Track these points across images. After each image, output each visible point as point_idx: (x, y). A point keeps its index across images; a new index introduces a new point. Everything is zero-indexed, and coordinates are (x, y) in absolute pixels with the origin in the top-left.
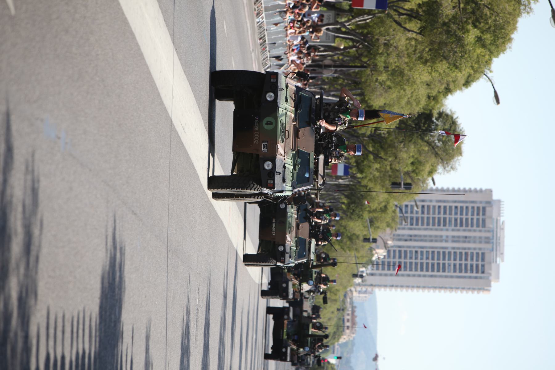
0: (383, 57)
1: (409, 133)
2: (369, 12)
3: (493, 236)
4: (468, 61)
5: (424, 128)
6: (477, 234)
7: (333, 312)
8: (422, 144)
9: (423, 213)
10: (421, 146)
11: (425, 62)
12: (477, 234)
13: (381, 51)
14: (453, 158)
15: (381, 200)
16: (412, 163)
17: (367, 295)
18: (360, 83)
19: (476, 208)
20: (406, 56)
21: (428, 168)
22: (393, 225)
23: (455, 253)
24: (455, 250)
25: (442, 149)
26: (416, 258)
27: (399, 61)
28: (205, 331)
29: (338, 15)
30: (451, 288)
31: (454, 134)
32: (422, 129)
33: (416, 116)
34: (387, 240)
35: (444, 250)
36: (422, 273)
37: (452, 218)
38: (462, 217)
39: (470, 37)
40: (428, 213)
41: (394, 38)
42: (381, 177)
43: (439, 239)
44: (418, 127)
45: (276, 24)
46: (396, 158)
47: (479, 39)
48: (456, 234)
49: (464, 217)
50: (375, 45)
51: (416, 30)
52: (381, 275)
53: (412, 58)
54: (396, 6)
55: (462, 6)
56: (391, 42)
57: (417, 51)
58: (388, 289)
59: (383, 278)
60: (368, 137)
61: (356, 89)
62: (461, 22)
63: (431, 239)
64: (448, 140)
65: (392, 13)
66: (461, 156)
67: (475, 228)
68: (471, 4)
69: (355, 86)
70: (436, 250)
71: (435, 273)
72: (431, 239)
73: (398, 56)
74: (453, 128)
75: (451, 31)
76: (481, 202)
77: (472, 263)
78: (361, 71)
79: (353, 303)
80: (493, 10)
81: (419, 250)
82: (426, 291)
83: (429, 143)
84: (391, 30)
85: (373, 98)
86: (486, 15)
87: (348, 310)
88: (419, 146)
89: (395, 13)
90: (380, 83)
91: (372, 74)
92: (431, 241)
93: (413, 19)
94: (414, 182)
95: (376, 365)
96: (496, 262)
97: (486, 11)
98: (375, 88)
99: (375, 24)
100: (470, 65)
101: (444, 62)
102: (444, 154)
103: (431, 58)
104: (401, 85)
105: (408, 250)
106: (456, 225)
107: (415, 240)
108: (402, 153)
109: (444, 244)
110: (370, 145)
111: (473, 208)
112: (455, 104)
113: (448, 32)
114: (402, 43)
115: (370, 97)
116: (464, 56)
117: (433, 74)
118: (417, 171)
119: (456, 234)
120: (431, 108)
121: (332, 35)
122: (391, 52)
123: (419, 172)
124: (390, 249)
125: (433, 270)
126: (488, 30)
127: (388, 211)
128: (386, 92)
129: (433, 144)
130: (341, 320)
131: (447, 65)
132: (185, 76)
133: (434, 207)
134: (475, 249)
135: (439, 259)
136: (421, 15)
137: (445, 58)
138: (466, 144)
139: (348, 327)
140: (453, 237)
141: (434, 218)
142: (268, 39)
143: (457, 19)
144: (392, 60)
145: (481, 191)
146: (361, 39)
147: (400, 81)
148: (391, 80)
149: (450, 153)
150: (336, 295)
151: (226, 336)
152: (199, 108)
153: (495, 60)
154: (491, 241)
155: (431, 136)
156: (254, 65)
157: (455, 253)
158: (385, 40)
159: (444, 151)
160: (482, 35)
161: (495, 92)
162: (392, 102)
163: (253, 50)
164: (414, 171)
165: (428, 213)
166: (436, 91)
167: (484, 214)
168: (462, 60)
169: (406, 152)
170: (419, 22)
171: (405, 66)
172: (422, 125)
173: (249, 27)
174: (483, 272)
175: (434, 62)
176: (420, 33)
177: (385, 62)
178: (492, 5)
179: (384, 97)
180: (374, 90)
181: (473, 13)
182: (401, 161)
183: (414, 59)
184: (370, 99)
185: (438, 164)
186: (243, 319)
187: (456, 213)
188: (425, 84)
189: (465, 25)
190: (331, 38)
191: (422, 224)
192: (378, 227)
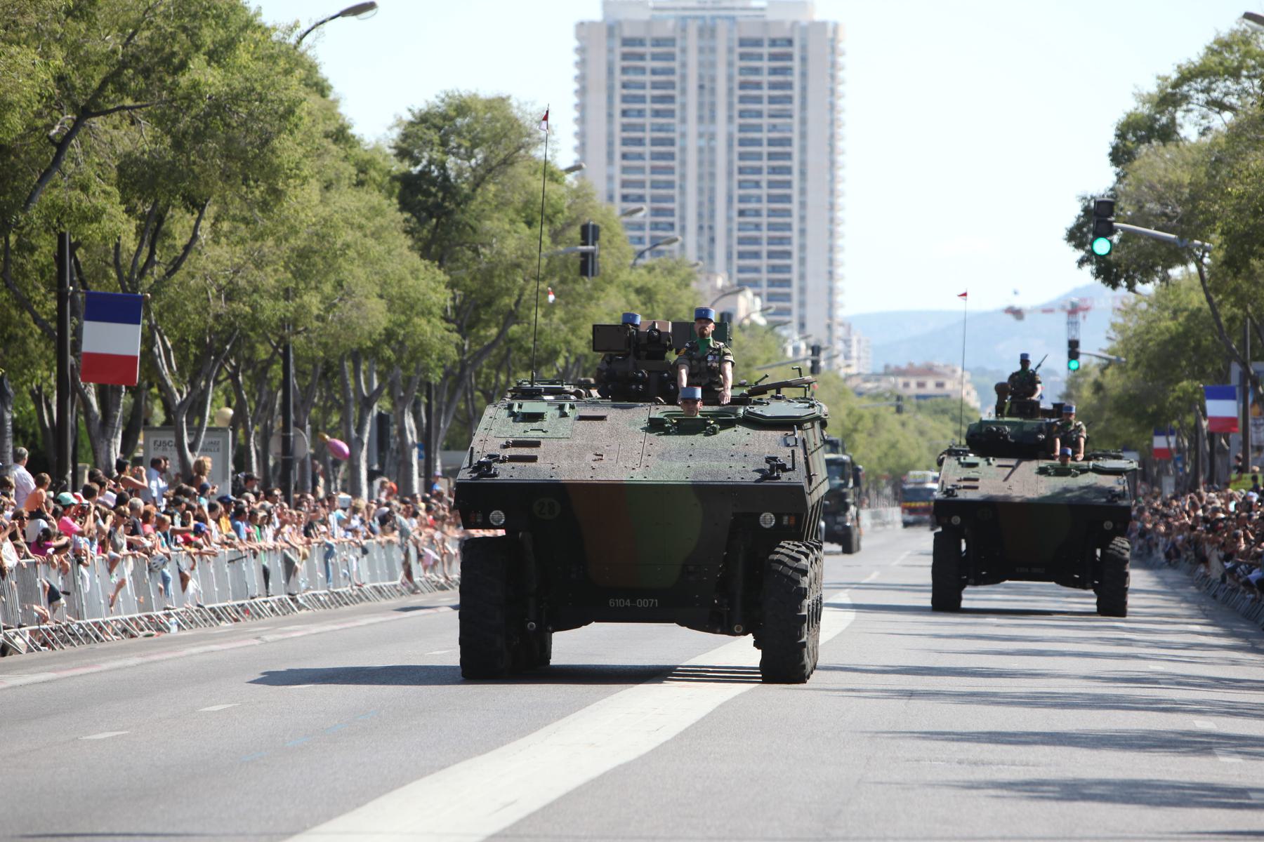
2: (148, 341)
3: (696, 18)
5: (440, 195)
6: (693, 58)
7: (903, 424)
8: (479, 199)
9: (641, 198)
10: (486, 202)
11: (277, 194)
12: (693, 58)
13: (247, 309)
15: (623, 301)
16: (529, 224)
17: (854, 339)
18: (327, 362)
19: (626, 63)
20: (259, 244)
21: (536, 184)
22: (683, 272)
23: (742, 114)
24: (736, 114)
26: (757, 213)
27: (274, 262)
28: (1011, 743)
29: (146, 422)
30: (832, 123)
31: (436, 127)
32: (444, 199)
33: (407, 215)
34: (714, 287)
35: (736, 142)
37: (652, 124)
39: (211, 80)
41: (213, 276)
42: (567, 303)
44: (437, 210)
45: (184, 580)
46: (518, 266)
47: (214, 57)
48: (692, 113)
49: (649, 92)
50: (232, 324)
51: (190, 220)
52: (802, 304)
54: (132, 272)
55: (129, 102)
56: (223, 282)
57: (248, 214)
58: (839, 285)
59: (810, 298)
60: (464, 338)
61: (342, 372)
65: (148, 281)
66: (509, 97)
69: (334, 376)
70: (737, 163)
71: (795, 164)
73: (259, 265)
74: (438, 121)
75: (196, 128)
76: (610, 50)
77: (766, 71)
78: (297, 358)
79: (874, 374)
80: (139, 21)
81: (737, 206)
82: (840, 187)
83: (479, 182)
84: (192, 282)
85: (367, 328)
86: (151, 39)
88: (487, 207)
90: (327, 310)
91: (306, 329)
92: (712, 176)
93: (164, 227)
94: (578, 218)
95: (1033, 310)
96: (762, 9)
97: (143, 38)
99: (176, 325)
101: (276, 143)
104: (335, 256)
105: (736, 234)
106: (671, 113)
108: (506, 252)
109: (721, 144)
110: (482, 333)
111: (625, 70)
112: (375, 118)
113: (199, 136)
116: (260, 94)
117: (305, 173)
118: (549, 211)
119: (692, 113)
122: (249, 282)
123: (552, 206)
124: (735, 281)
125: (788, 170)
126: (192, 34)
128: (350, 294)
129: (481, 171)
130: (922, 402)
131: (283, 136)
133: (625, 170)
136: (155, 205)
138: (479, 83)
139: (940, 385)
140: (701, 119)
141: (655, 170)
143: (164, 114)
144: (270, 279)
145: (581, 50)
146: (215, 361)
147: (324, 258)
148: (320, 282)
149: (503, 128)
150: (861, 418)
151: (1008, 690)
152: (443, 767)
153: (267, 19)
154: (709, 22)
155: (459, 175)
156: (294, 635)
157: (742, 114)
159: (497, 143)
160: (204, 50)
161: (344, 13)
162: (376, 278)
165: (641, 184)
166: (345, 165)
167: (641, 42)
168: (269, 97)
171: (285, 246)
172: (431, 200)
173: (201, 649)
174: (790, 42)
175: (275, 171)
177: (275, 298)
178: (126, 25)
180: (347, 326)
181: (146, 72)
182: (527, 252)
183: (269, 224)
184: (370, 334)
185: (531, 158)
187: (640, 113)
188: (328, 195)
189: (180, 92)
191: (671, 199)
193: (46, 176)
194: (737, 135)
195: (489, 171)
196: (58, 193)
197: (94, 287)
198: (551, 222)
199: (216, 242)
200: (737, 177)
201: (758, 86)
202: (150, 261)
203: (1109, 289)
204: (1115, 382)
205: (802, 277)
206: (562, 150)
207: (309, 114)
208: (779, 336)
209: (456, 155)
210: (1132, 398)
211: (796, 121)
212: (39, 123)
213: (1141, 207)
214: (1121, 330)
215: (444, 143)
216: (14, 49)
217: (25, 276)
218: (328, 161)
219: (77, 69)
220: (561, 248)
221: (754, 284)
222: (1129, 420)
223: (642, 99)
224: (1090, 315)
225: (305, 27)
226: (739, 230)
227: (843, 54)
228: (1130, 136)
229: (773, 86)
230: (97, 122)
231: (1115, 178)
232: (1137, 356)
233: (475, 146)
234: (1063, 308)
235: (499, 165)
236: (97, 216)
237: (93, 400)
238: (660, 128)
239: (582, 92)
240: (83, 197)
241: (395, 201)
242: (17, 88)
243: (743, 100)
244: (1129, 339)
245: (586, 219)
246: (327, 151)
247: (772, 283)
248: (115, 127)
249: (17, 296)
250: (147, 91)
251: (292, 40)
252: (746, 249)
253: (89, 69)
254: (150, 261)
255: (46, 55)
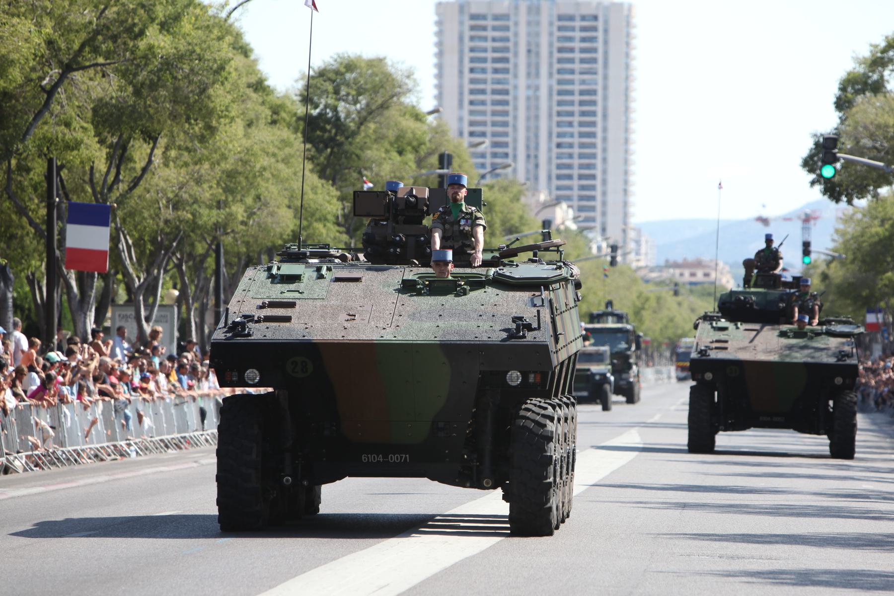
0: (201, 211)
1: (344, 160)
4: (209, 47)
5: (334, 131)
6: (523, 30)
7: (679, 304)
8: (363, 134)
9: (483, 134)
10: (367, 136)
11: (211, 130)
12: (523, 30)
13: (189, 216)
14: (390, 75)
16: (400, 153)
17: (643, 240)
19: (473, 33)
20: (197, 167)
21: (409, 124)
22: (515, 190)
25: (373, 96)
26: (571, 146)
27: (208, 181)
28: (758, 542)
29: (113, 301)
30: (627, 78)
32: (336, 134)
33: (308, 146)
34: (538, 201)
36: (600, 135)
37: (493, 79)
38: (489, 60)
39: (162, 44)
40: (484, 124)
41: (164, 191)
43: (533, 102)
44: (331, 142)
49: (490, 55)
50: (177, 228)
52: (604, 214)
53: (203, 155)
55: (101, 60)
56: (171, 195)
57: (190, 145)
58: (632, 199)
59: (610, 209)
60: (351, 237)
62: (132, 60)
63: (533, 117)
64: (355, 84)
65: (115, 195)
66: (385, 58)
67: (510, 34)
68: (97, 43)
70: (556, 108)
71: (599, 109)
72: (533, 117)
73: (198, 182)
74: (332, 76)
75: (151, 80)
76: (461, 23)
78: (226, 252)
81: (555, 140)
83: (362, 122)
84: (148, 196)
86: (118, 13)
87: (673, 275)
89: (115, 191)
90: (249, 217)
91: (233, 231)
92: (537, 117)
93: (126, 155)
94: (436, 149)
95: (776, 219)
97: (111, 13)
98: (259, 225)
99: (135, 227)
100: (216, 43)
101: (211, 91)
102: (382, 90)
103: (204, 118)
104: (255, 177)
106: (506, 71)
107: (537, 147)
108: (383, 174)
109: (543, 93)
113: (153, 86)
114: (174, 176)
115: (278, 236)
116: (199, 55)
117: (233, 114)
118: (415, 143)
120: (294, 119)
121: (158, 311)
122: (190, 195)
123: (417, 139)
124: (553, 196)
125: (594, 114)
127: (491, 199)
128: (266, 204)
129: (364, 113)
130: (693, 287)
131: (217, 86)
132: (279, 587)
133: (472, 113)
134: (551, 34)
135: (572, 103)
136: (120, 137)
137: (203, 91)
138: (363, 48)
139: (706, 275)
140: (529, 75)
141: (494, 113)
142: (168, 434)
143: (127, 70)
144: (206, 193)
145: (439, 23)
147: (247, 178)
148: (243, 196)
149: (381, 81)
150: (647, 299)
151: (756, 503)
157: (559, 71)
158: (167, 207)
160: (157, 21)
162: (286, 193)
163: (196, 462)
164: (416, 150)
165: (484, 124)
166: (263, 108)
168: (206, 57)
169: (380, 165)
170: (132, 142)
171: (217, 169)
172: (327, 135)
174: (595, 18)
175: (210, 113)
176: (155, 140)
177: (210, 207)
179: (276, 209)
181: (114, 38)
182: (398, 174)
183: (205, 152)
184: (281, 235)
185: (401, 104)
186: (721, 472)
187: (484, 71)
188: (250, 131)
190: (163, 313)
191: (506, 134)
192: (521, 217)
193: (38, 115)
194: (556, 87)
195: (370, 113)
196: (48, 128)
197: (74, 199)
198: (417, 151)
199: (166, 165)
200: (556, 119)
201: (572, 50)
202: (117, 180)
203: (834, 203)
204: (837, 273)
205: (604, 193)
206: (424, 97)
207: (236, 70)
208: (586, 238)
209: (346, 101)
210: (850, 284)
211: (599, 78)
212: (34, 76)
213: (858, 142)
214: (843, 234)
215: (337, 92)
216: (15, 20)
217: (23, 190)
218: (249, 105)
219: (63, 35)
220: (424, 171)
221: (568, 198)
222: (849, 301)
223: (484, 60)
224: (819, 222)
225: (233, 5)
226: (558, 158)
227: (635, 27)
228: (850, 89)
229: (583, 50)
230: (77, 75)
231: (838, 121)
232: (854, 253)
233: (359, 94)
234: (799, 218)
235: (378, 108)
236: (76, 145)
237: (74, 283)
238: (499, 82)
239: (440, 54)
240: (66, 131)
241: (299, 135)
242: (17, 50)
243: (560, 61)
244: (848, 241)
245: (443, 150)
246: (249, 98)
247: (581, 198)
248: (91, 79)
249: (16, 205)
250: (115, 52)
251: (223, 15)
252: (563, 173)
253: (72, 36)
254: (117, 180)
255: (39, 25)
